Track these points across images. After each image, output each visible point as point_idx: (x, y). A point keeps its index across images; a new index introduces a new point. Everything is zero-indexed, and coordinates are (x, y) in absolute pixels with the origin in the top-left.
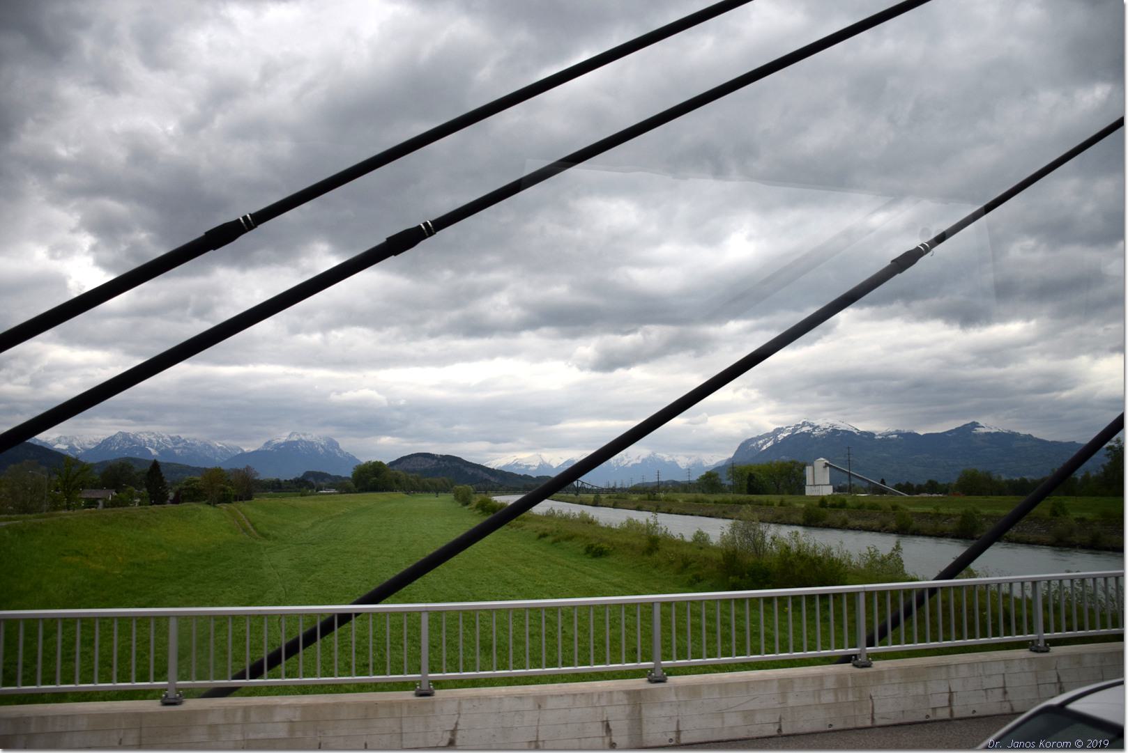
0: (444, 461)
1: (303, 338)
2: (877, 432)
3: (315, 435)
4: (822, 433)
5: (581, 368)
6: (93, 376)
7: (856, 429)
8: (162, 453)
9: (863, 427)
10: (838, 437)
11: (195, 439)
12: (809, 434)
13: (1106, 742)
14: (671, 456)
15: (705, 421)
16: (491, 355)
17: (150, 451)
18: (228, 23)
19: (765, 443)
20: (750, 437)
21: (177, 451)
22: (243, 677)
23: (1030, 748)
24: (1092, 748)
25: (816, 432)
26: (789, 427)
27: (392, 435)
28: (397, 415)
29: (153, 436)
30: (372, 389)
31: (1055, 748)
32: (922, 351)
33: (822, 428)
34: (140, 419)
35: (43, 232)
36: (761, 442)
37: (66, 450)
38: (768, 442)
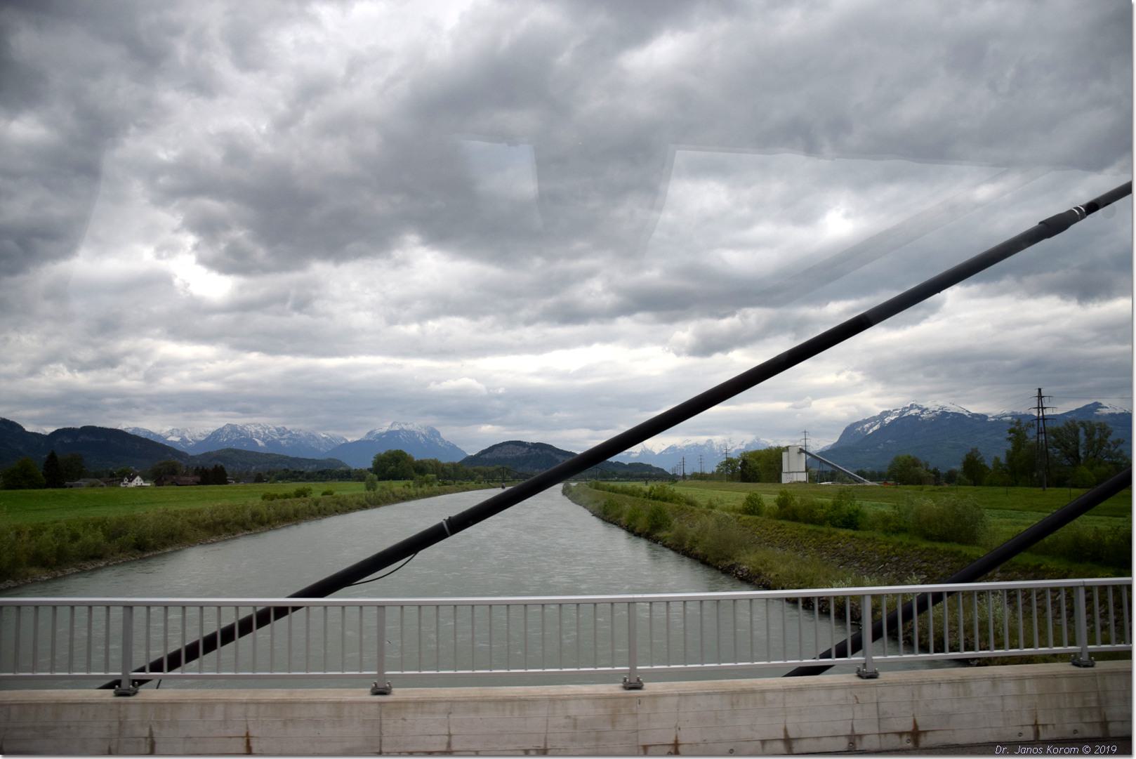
0: (536, 448)
1: (401, 329)
2: (990, 414)
3: (416, 424)
4: (930, 416)
5: (678, 354)
6: (201, 370)
7: (967, 411)
8: (268, 443)
9: (975, 409)
10: (948, 419)
11: (301, 430)
12: (917, 417)
13: (1114, 748)
14: (775, 441)
15: (809, 404)
16: (589, 341)
17: (256, 442)
18: (314, 20)
19: (871, 427)
20: (856, 421)
21: (282, 442)
22: (829, 657)
23: (1038, 754)
24: (1100, 754)
25: (925, 415)
26: (897, 410)
27: (493, 424)
28: (497, 403)
29: (259, 428)
30: (470, 377)
31: (1062, 754)
32: (1037, 328)
33: (931, 410)
34: (246, 411)
35: (150, 233)
36: (867, 426)
37: (179, 442)
38: (874, 426)
